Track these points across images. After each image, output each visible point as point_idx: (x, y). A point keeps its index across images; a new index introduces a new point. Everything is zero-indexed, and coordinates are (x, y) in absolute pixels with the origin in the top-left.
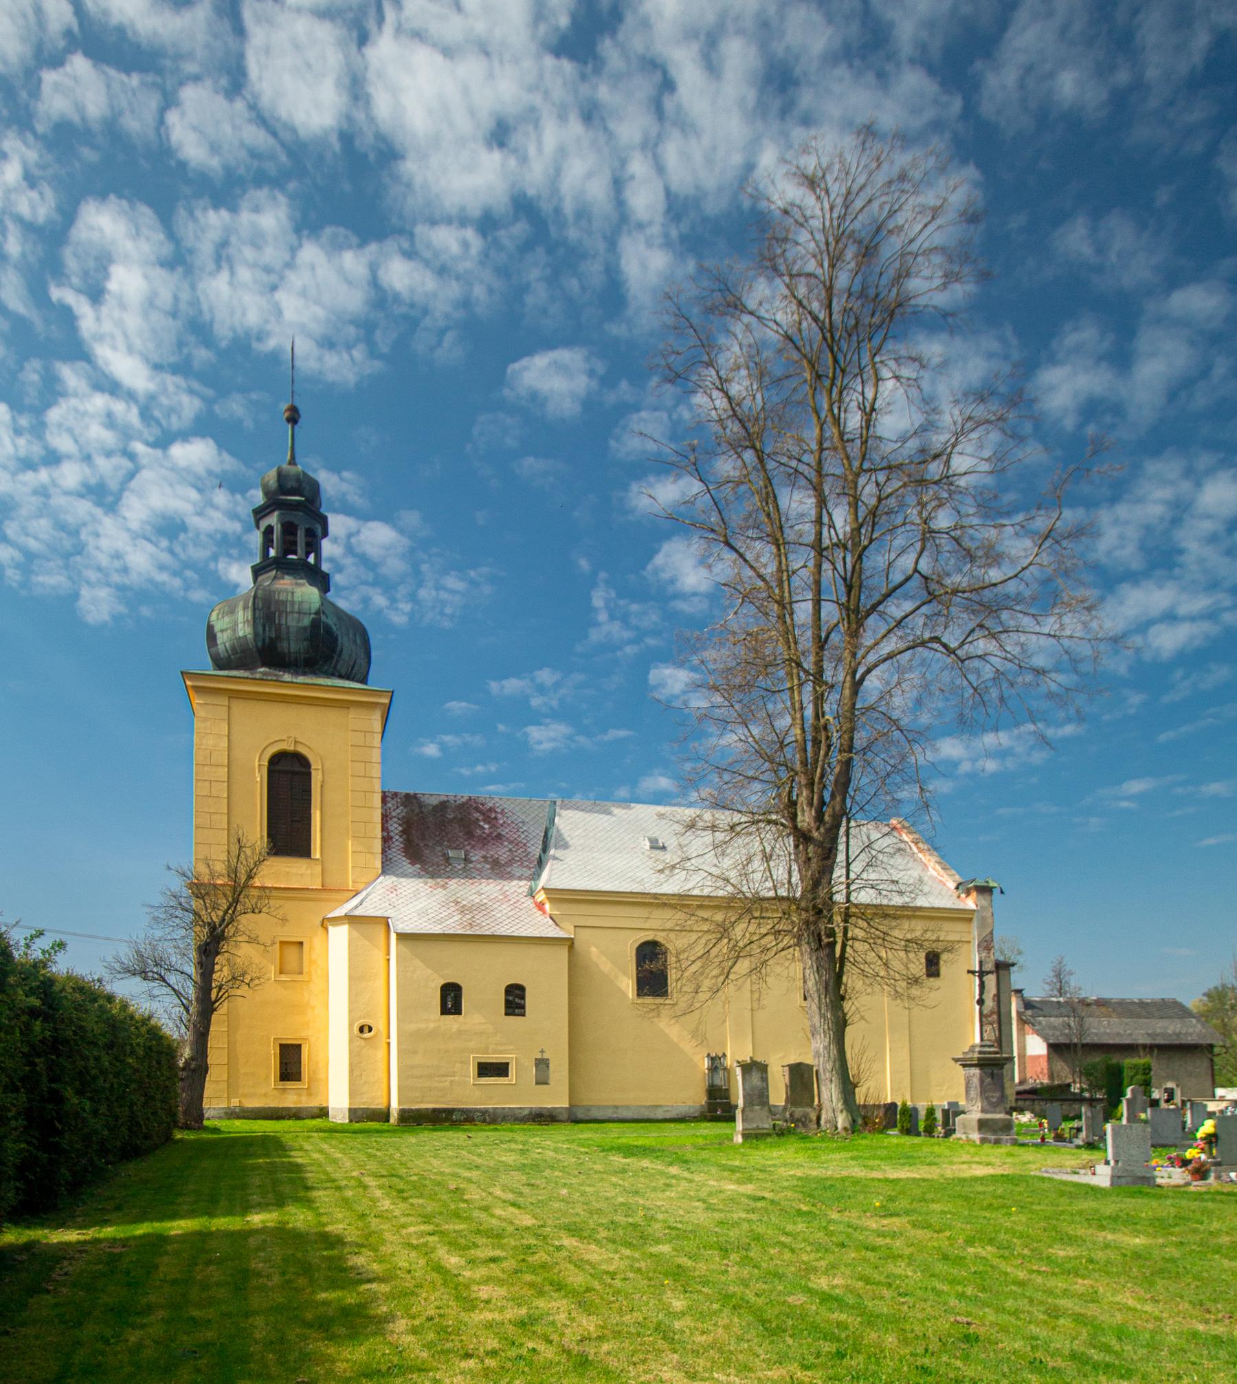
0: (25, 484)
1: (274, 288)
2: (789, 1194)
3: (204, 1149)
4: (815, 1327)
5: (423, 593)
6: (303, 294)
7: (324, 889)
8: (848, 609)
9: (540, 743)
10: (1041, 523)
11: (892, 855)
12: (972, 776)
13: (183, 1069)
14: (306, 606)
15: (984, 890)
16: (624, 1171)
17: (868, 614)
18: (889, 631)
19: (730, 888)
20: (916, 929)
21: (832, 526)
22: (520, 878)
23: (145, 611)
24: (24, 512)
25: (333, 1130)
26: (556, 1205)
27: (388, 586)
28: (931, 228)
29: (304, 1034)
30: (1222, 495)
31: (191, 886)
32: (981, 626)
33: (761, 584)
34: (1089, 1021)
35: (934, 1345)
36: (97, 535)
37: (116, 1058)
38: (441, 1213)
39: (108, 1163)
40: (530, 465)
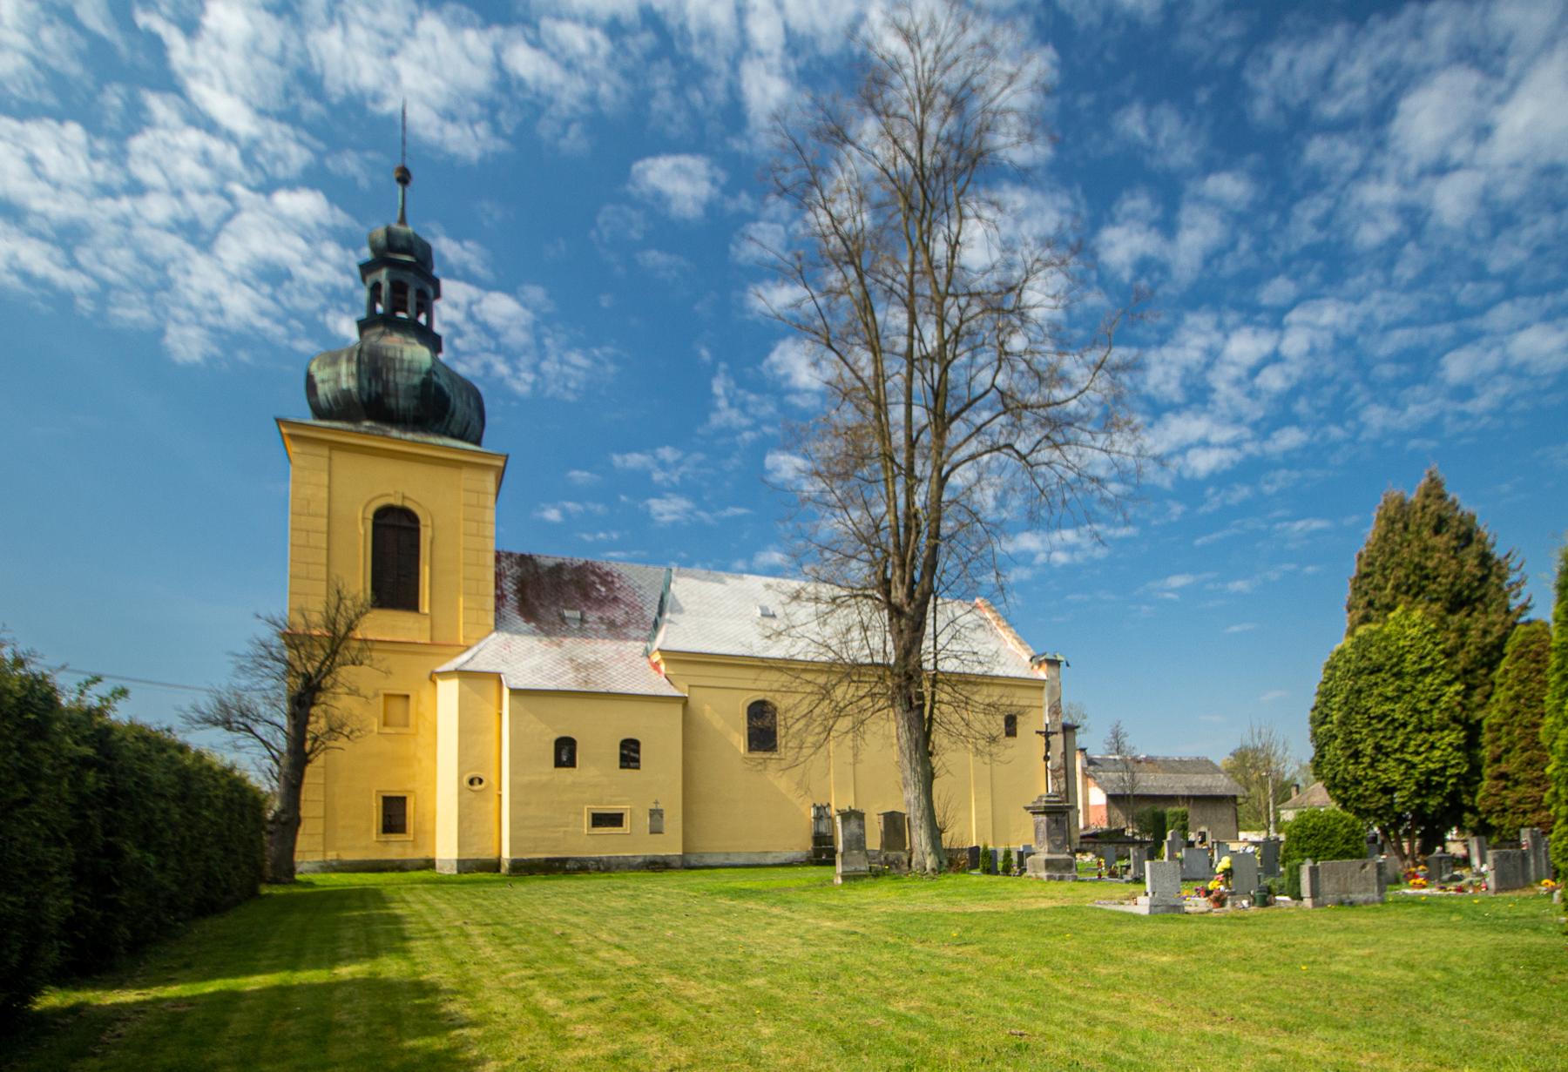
0: (103, 211)
1: (391, 53)
2: (880, 928)
3: (291, 903)
4: (889, 1045)
5: (546, 366)
6: (423, 63)
7: (432, 644)
8: (935, 414)
9: (661, 515)
10: (1096, 355)
11: (974, 630)
12: (1047, 565)
13: (272, 822)
14: (416, 365)
15: (1054, 663)
16: (729, 912)
17: (952, 419)
18: (970, 436)
19: (831, 655)
20: (994, 695)
21: (921, 340)
22: (636, 639)
23: (243, 356)
25: (441, 882)
26: (661, 946)
27: (510, 356)
28: (1007, 91)
29: (409, 787)
31: (283, 635)
32: (1047, 437)
33: (859, 384)
34: (1138, 776)
35: (990, 1055)
36: (188, 272)
37: (189, 812)
38: (544, 958)
39: (178, 920)
40: (654, 257)
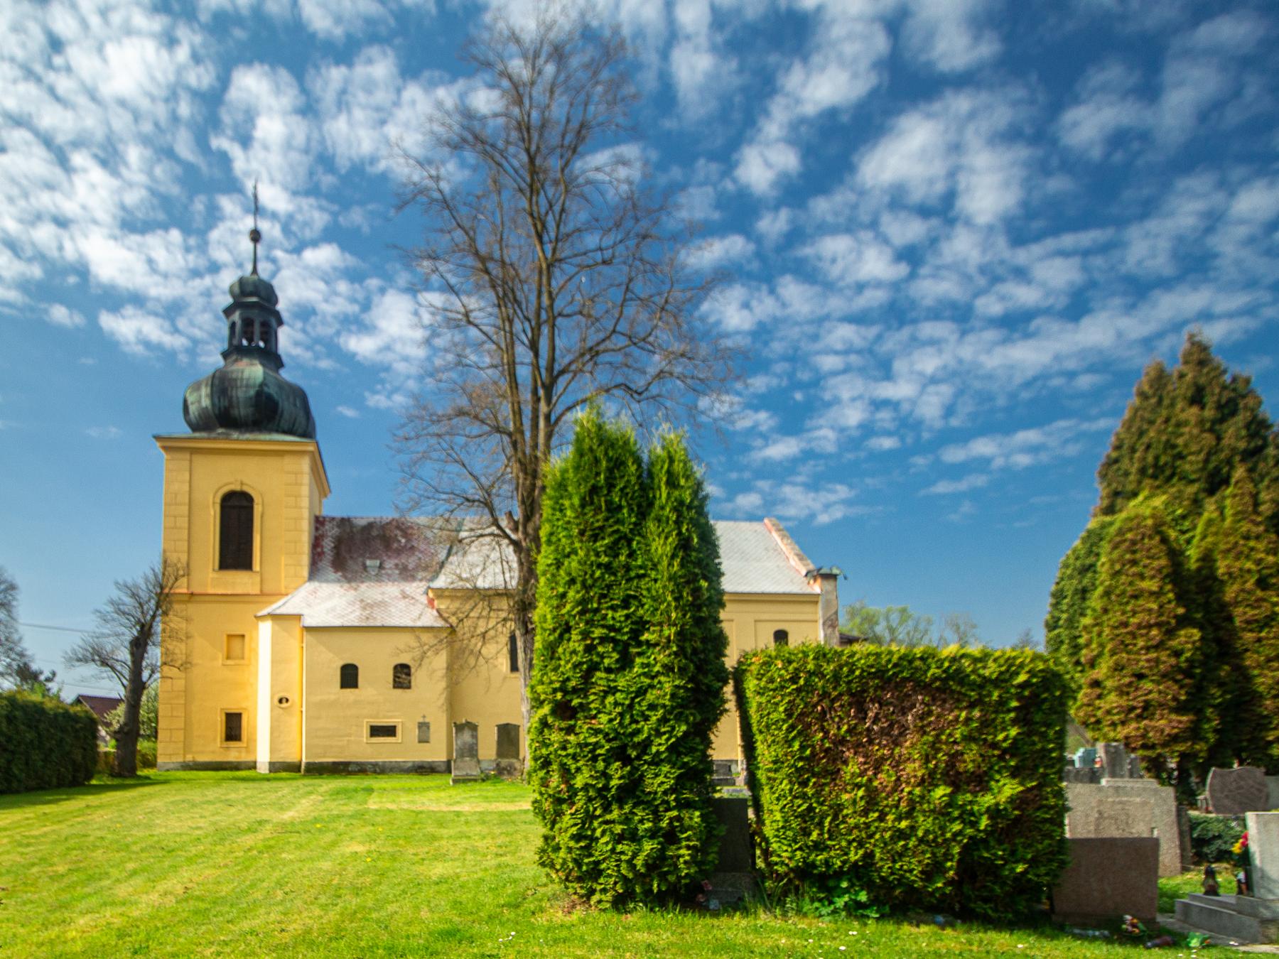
0: (193, 288)
1: (383, 122)
7: (262, 594)
12: (1005, 470)
14: (251, 382)
24: (192, 310)
29: (244, 705)
30: (1255, 202)
